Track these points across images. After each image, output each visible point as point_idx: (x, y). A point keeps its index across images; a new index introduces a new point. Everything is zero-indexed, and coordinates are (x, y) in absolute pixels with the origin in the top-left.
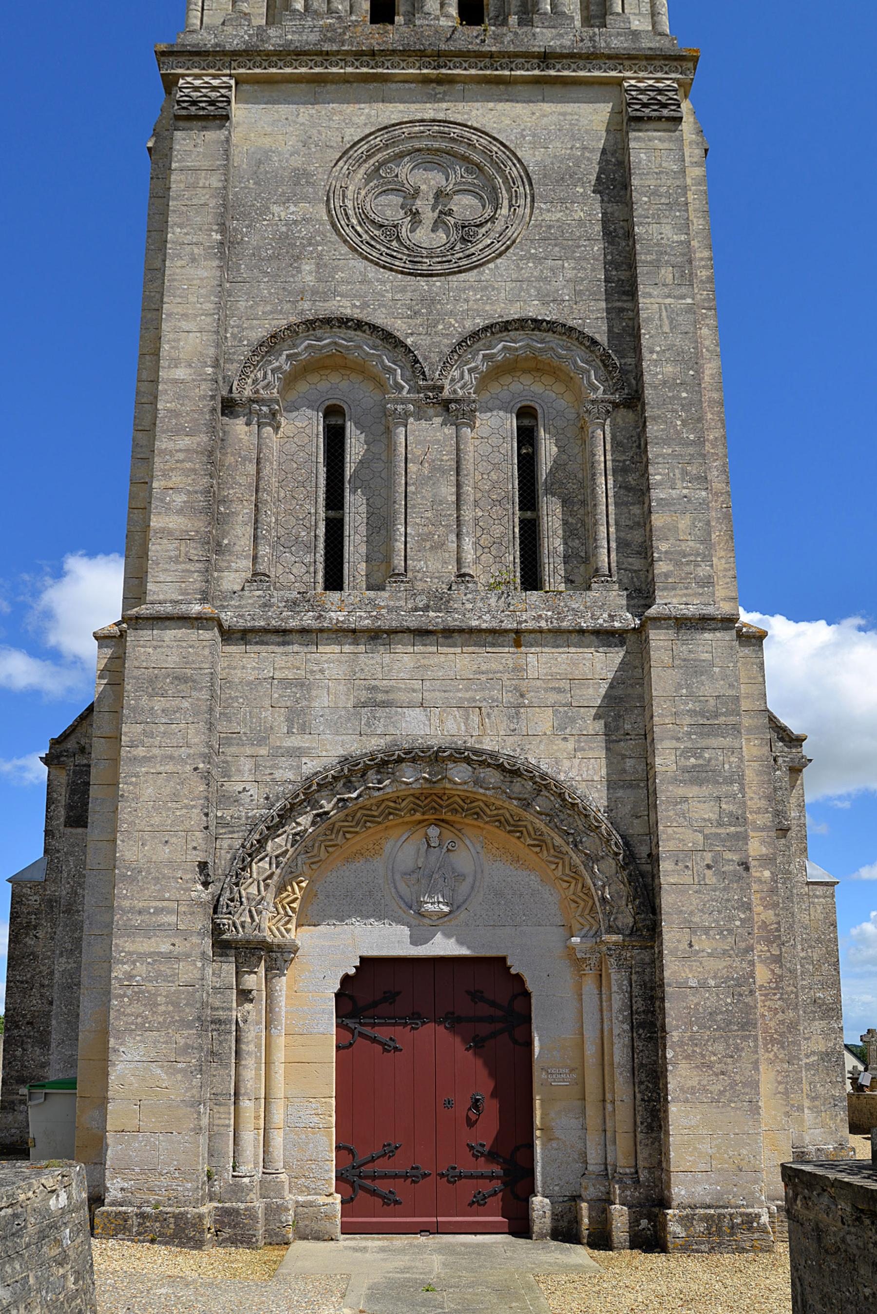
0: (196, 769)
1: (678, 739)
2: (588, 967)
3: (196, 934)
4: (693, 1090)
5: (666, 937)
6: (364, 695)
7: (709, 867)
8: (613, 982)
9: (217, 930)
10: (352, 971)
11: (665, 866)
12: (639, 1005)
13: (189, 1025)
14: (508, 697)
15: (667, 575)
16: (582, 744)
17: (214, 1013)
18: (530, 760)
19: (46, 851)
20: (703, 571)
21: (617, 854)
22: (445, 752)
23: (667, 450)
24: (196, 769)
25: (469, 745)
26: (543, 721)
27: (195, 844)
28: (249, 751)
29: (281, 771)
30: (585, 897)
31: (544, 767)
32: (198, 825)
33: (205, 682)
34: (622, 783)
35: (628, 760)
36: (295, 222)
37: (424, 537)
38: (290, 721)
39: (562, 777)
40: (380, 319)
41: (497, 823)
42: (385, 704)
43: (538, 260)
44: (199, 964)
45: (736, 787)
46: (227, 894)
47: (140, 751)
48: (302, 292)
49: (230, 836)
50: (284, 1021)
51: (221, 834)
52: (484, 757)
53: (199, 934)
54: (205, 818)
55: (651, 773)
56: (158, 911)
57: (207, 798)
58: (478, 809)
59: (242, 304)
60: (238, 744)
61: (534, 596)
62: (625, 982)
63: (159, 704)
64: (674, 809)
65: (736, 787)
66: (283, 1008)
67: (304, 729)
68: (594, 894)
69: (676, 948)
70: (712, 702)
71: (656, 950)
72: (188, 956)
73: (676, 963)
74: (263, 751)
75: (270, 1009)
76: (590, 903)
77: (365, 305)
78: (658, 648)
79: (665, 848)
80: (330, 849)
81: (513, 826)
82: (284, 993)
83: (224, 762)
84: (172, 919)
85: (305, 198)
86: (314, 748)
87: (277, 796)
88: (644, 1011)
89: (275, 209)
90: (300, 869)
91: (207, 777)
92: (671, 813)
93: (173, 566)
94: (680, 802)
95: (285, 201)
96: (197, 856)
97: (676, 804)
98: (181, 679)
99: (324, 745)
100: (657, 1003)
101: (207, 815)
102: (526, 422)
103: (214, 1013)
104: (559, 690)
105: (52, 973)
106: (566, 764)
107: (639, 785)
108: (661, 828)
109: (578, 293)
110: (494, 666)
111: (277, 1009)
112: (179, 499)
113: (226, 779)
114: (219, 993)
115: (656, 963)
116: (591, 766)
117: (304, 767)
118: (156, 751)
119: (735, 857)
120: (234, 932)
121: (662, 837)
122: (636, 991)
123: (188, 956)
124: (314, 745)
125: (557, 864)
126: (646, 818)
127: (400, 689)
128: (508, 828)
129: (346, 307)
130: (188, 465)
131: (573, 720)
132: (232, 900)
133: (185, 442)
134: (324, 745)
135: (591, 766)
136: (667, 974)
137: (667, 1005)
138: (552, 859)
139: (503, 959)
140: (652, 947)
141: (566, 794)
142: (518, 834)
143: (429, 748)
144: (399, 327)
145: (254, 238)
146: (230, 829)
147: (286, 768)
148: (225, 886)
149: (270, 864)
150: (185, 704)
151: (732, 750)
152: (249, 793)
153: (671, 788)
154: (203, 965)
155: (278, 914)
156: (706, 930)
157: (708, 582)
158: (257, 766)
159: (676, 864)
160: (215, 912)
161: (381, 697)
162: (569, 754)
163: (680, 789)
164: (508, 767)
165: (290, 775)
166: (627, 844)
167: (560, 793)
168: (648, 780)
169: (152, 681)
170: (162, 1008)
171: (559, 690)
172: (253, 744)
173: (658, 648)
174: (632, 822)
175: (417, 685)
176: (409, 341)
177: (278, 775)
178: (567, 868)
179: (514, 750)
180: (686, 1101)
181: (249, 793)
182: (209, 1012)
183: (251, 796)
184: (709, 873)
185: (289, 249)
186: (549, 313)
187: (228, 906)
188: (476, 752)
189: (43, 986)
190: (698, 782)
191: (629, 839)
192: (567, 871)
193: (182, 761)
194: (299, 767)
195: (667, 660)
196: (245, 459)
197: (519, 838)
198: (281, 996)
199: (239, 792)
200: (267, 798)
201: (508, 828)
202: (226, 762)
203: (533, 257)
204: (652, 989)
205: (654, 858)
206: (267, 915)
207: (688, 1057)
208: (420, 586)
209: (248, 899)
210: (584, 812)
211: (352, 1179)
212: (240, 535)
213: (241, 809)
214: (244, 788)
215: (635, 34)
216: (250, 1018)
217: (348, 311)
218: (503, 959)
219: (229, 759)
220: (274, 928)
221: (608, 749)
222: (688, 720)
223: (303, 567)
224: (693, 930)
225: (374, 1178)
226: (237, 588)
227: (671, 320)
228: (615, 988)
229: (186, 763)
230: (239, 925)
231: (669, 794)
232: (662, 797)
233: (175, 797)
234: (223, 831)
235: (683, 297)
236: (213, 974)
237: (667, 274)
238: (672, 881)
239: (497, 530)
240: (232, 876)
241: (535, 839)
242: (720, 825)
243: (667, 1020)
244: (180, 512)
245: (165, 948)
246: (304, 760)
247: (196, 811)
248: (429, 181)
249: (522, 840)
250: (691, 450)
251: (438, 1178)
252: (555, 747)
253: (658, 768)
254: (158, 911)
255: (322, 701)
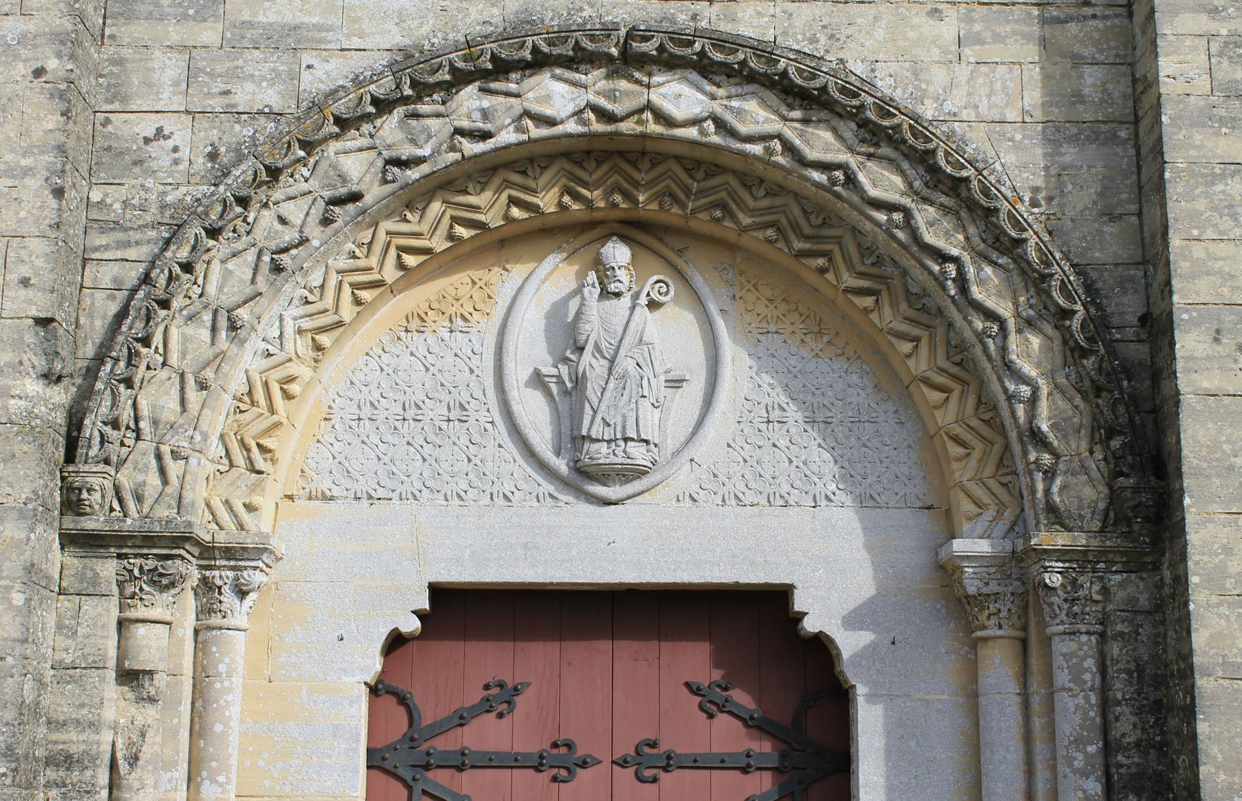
0: (39, 72)
2: (993, 620)
3: (15, 514)
5: (1196, 535)
8: (1058, 661)
11: (1189, 344)
12: (1126, 726)
16: (977, 27)
17: (55, 736)
18: (851, 66)
21: (1068, 314)
22: (646, 39)
24: (39, 72)
25: (704, 24)
27: (25, 271)
28: (174, 33)
29: (250, 87)
30: (985, 430)
31: (884, 85)
32: (36, 222)
34: (1074, 130)
35: (1087, 70)
39: (928, 111)
41: (770, 233)
44: (18, 599)
49: (119, 254)
50: (234, 761)
51: (96, 249)
52: (741, 56)
53: (22, 515)
54: (53, 203)
55: (1147, 102)
57: (61, 150)
58: (723, 195)
60: (149, 16)
62: (1090, 663)
64: (1207, 195)
66: (234, 724)
68: (1008, 421)
69: (1222, 569)
71: (1167, 575)
73: (1224, 610)
74: (209, 35)
75: (198, 729)
76: (997, 448)
80: (366, 295)
81: (808, 238)
82: (237, 680)
83: (114, 62)
86: (330, 29)
87: (238, 151)
88: (1138, 744)
90: (289, 346)
91: (67, 97)
92: (1201, 204)
94: (1223, 176)
96: (30, 302)
97: (1214, 179)
99: (358, 20)
100: (1173, 722)
101: (59, 193)
103: (55, 736)
106: (939, 76)
107: (1115, 136)
108: (1175, 242)
111: (218, 728)
113: (116, 106)
114: (73, 680)
115: (1169, 609)
116: (998, 85)
117: (306, 76)
120: (117, 513)
121: (1180, 266)
122: (1120, 687)
124: (333, 20)
125: (917, 339)
126: (1134, 219)
128: (798, 245)
132: (115, 424)
134: (358, 20)
135: (998, 85)
136: (1199, 639)
137: (1202, 727)
138: (904, 327)
140: (1156, 567)
141: (940, 154)
142: (821, 261)
143: (608, 30)
146: (119, 236)
147: (264, 78)
148: (99, 386)
149: (214, 329)
152: (170, 143)
153: (1198, 138)
154: (29, 600)
155: (232, 465)
158: (191, 73)
159: (1216, 340)
160: (70, 458)
162: (945, 52)
163: (1222, 141)
164: (799, 81)
165: (271, 97)
166: (1089, 287)
167: (926, 152)
168: (1137, 121)
172: (186, 17)
174: (1100, 232)
177: (245, 96)
178: (941, 352)
179: (813, 40)
181: (170, 143)
182: (42, 731)
183: (176, 149)
187: (103, 440)
191: (1094, 275)
192: (942, 362)
194: (295, 77)
197: (822, 271)
198: (229, 690)
199: (147, 141)
200: (213, 156)
201: (798, 245)
202: (119, 62)
204: (1159, 682)
205: (1158, 327)
206: (201, 467)
209: (155, 423)
210: (983, 202)
213: (149, 183)
214: (159, 130)
216: (146, 752)
219: (126, 53)
220: (217, 504)
221: (1044, 43)
228: (1062, 678)
229: (16, 57)
230: (128, 486)
231: (1193, 153)
232: (1177, 159)
234: (102, 240)
236: (60, 627)
238: (1206, 384)
240: (117, 360)
241: (861, 275)
243: (1203, 770)
246: (307, 59)
247: (34, 183)
249: (830, 276)
252: (911, 34)
253: (1168, 88)
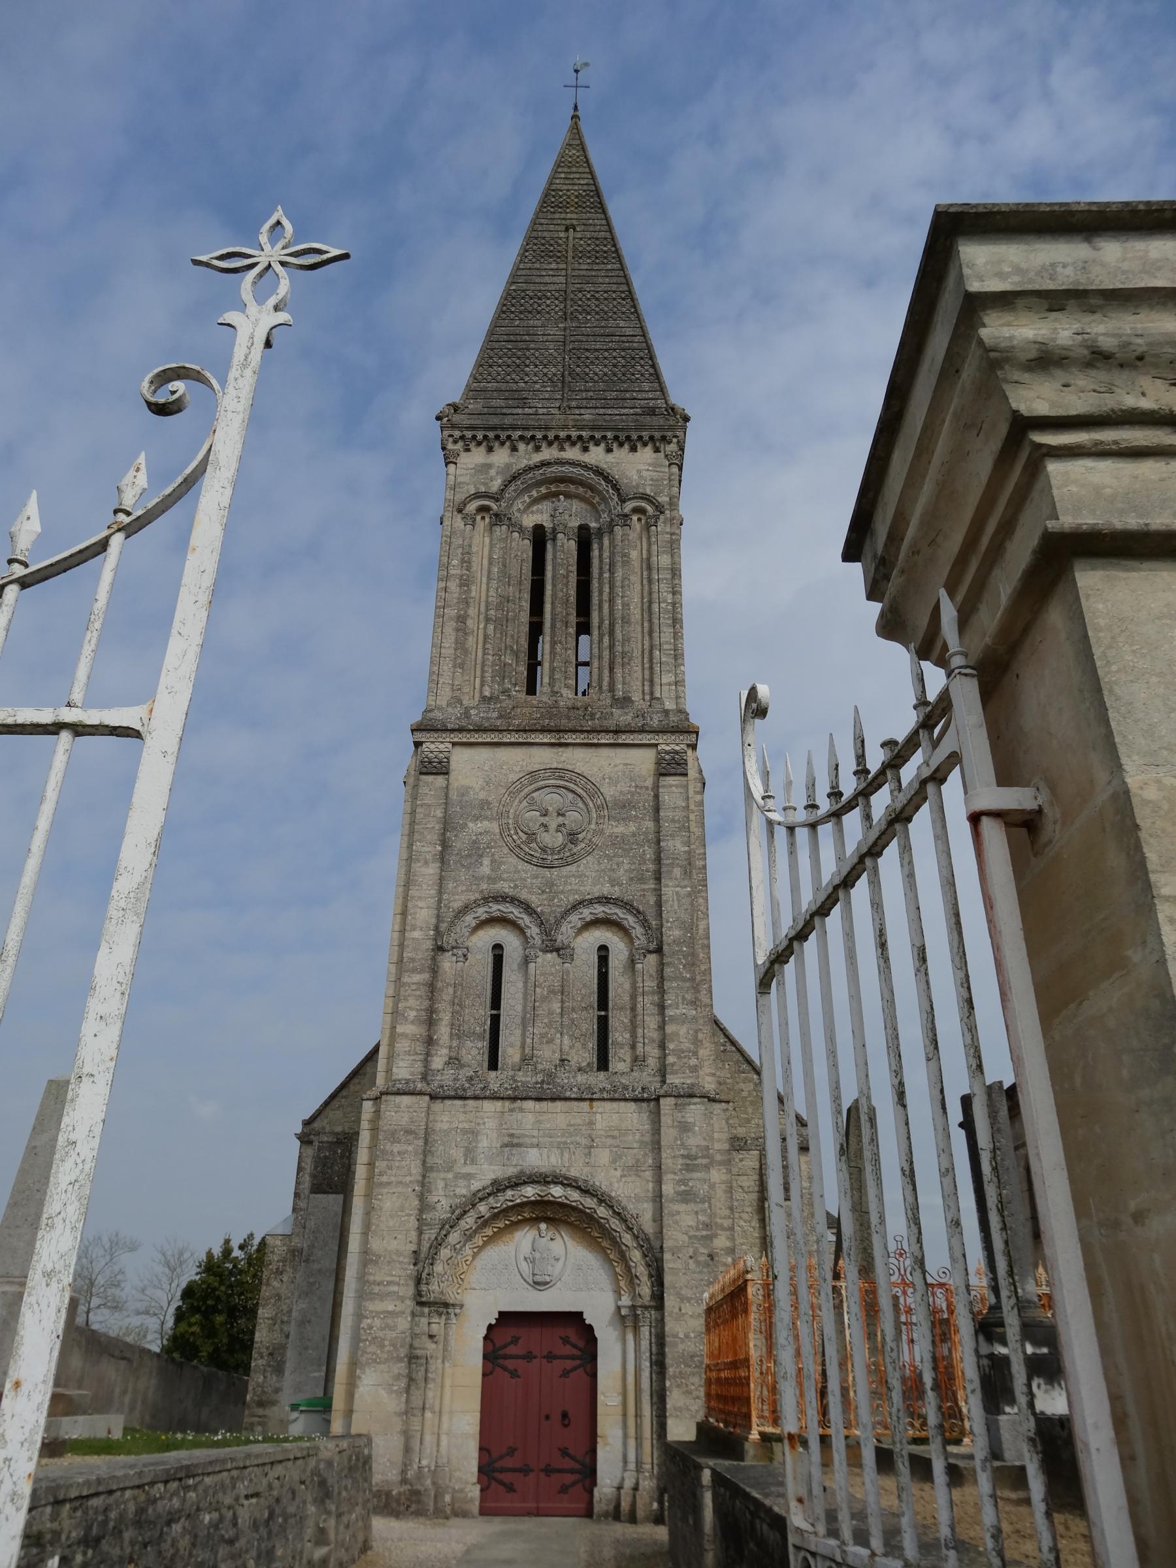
1: (675, 1173)
4: (680, 1409)
6: (506, 1140)
7: (691, 1257)
9: (419, 1293)
10: (494, 1322)
11: (667, 1256)
13: (400, 1360)
14: (584, 1141)
15: (673, 1065)
19: (294, 1210)
20: (693, 1062)
23: (675, 984)
26: (603, 1156)
33: (422, 1133)
36: (481, 834)
37: (543, 1036)
38: (466, 1156)
39: (613, 1194)
40: (524, 895)
42: (518, 1145)
43: (610, 858)
45: (706, 1205)
46: (426, 1271)
47: (384, 1179)
48: (482, 878)
56: (389, 1283)
59: (451, 885)
61: (602, 1075)
63: (396, 1148)
65: (706, 1205)
67: (473, 1162)
70: (694, 1149)
72: (403, 1313)
74: (450, 1176)
77: (516, 886)
78: (665, 1114)
79: (667, 1244)
84: (395, 1288)
85: (486, 818)
89: (471, 825)
93: (407, 1057)
95: (477, 818)
98: (408, 1132)
102: (603, 953)
104: (614, 1137)
105: (290, 1311)
106: (616, 1185)
109: (631, 879)
110: (579, 1121)
112: (412, 1014)
118: (393, 1179)
119: (706, 1252)
123: (403, 1313)
127: (526, 1136)
129: (505, 887)
130: (418, 993)
131: (621, 1158)
133: (417, 978)
139: (582, 1313)
144: (534, 900)
145: (460, 843)
150: (410, 1148)
151: (705, 1181)
156: (689, 1300)
157: (694, 1069)
161: (515, 1141)
165: (464, 1192)
169: (393, 1133)
170: (387, 1349)
171: (614, 1137)
173: (665, 1114)
175: (535, 1133)
176: (539, 910)
180: (677, 1416)
184: (691, 1261)
185: (477, 851)
186: (616, 892)
188: (566, 1178)
189: (282, 1322)
190: (686, 1201)
193: (407, 1185)
195: (670, 1122)
196: (448, 984)
203: (608, 855)
207: (678, 1386)
208: (540, 1067)
211: (487, 1471)
212: (443, 1032)
215: (666, 712)
217: (507, 890)
218: (582, 1313)
222: (680, 1161)
223: (474, 1052)
224: (682, 1300)
225: (501, 1472)
226: (440, 1067)
227: (679, 901)
233: (402, 1209)
235: (686, 887)
237: (677, 872)
239: (584, 1027)
242: (698, 1229)
244: (412, 1022)
245: (391, 1308)
248: (552, 800)
250: (688, 984)
251: (542, 1474)
254: (389, 1283)
255: (484, 1143)
